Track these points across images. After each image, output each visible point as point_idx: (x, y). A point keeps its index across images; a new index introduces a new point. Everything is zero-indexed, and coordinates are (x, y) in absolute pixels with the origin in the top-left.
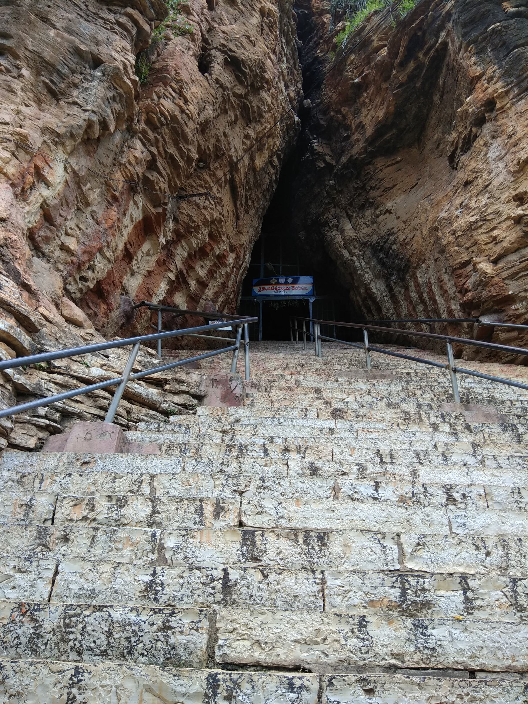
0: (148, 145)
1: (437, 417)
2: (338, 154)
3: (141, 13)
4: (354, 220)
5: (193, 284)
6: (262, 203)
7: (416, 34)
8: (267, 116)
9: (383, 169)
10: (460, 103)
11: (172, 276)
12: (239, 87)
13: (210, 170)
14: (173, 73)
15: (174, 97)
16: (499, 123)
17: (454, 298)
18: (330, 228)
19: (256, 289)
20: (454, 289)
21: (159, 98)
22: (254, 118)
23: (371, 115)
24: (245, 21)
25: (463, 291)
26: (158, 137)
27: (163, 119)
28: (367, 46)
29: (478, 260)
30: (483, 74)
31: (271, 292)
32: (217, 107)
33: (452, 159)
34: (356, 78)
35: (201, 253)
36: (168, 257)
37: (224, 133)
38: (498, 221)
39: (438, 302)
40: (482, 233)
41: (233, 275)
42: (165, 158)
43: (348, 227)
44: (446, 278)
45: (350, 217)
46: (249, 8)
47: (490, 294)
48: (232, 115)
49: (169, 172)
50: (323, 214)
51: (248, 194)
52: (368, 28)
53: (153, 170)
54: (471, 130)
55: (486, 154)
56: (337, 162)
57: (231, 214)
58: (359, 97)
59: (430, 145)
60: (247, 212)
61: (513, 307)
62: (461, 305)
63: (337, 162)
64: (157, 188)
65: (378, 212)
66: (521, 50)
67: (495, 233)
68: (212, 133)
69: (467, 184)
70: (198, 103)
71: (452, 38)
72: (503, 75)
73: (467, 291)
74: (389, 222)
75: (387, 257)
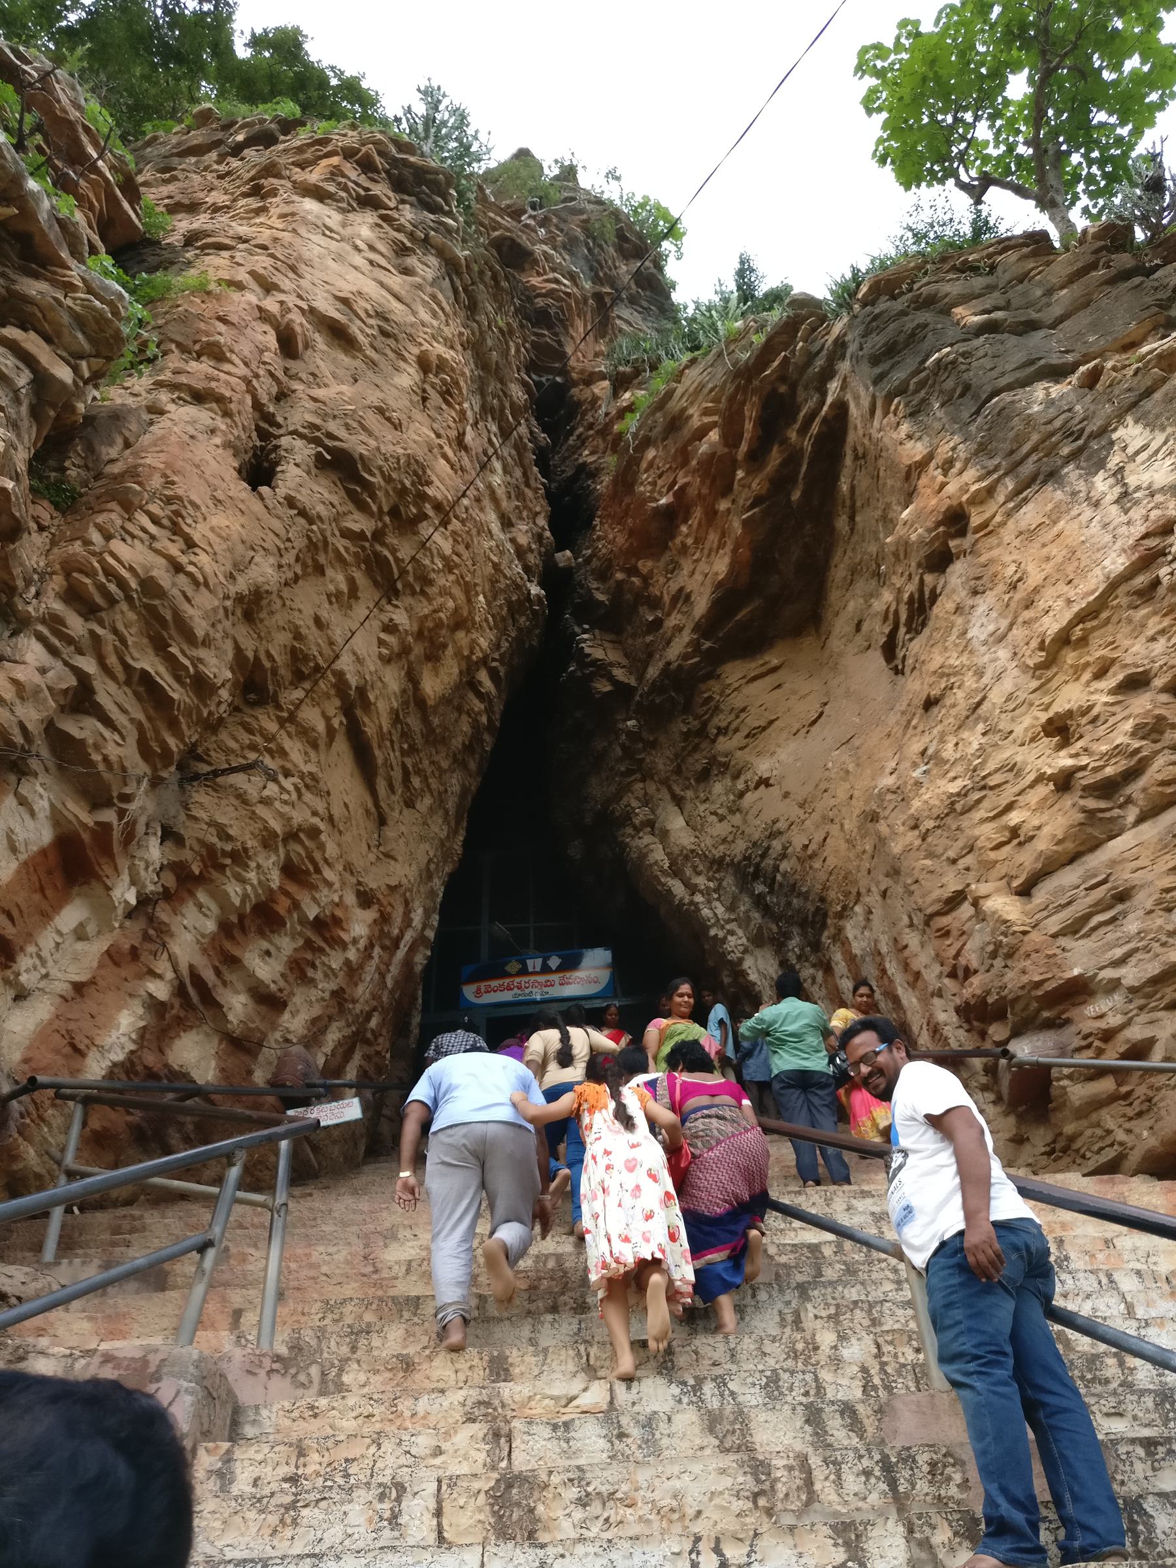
0: (66, 651)
1: (867, 1473)
2: (639, 664)
3: (48, 340)
4: (688, 806)
5: (237, 1006)
6: (455, 783)
7: (774, 390)
8: (442, 581)
9: (743, 688)
10: (888, 522)
11: (160, 990)
12: (357, 515)
13: (279, 707)
14: (156, 482)
15: (153, 537)
16: (983, 559)
17: (939, 993)
18: (635, 828)
19: (469, 991)
20: (937, 969)
21: (108, 537)
22: (407, 585)
23: (701, 573)
24: (379, 381)
25: (960, 973)
26: (100, 631)
27: (112, 587)
28: (680, 428)
29: (982, 889)
30: (930, 457)
31: (507, 996)
32: (289, 558)
33: (890, 650)
34: (661, 494)
35: (264, 917)
36: (146, 937)
37: (318, 621)
38: (1017, 789)
39: (905, 1002)
40: (984, 821)
41: (371, 968)
42: (128, 683)
43: (676, 823)
44: (912, 939)
45: (679, 801)
46: (391, 355)
47: (1025, 979)
48: (340, 577)
49: (141, 716)
50: (618, 797)
51: (409, 762)
52: (678, 393)
53: (87, 713)
54: (922, 581)
55: (965, 633)
56: (640, 678)
57: (358, 813)
58: (672, 537)
59: (841, 626)
60: (410, 804)
61: (1091, 1010)
62: (958, 1010)
63: (640, 678)
64: (96, 757)
65: (740, 785)
66: (1006, 397)
67: (1014, 818)
68: (280, 618)
69: (930, 704)
70: (230, 550)
71: (852, 387)
72: (976, 453)
73: (968, 973)
74: (766, 807)
75: (771, 892)
